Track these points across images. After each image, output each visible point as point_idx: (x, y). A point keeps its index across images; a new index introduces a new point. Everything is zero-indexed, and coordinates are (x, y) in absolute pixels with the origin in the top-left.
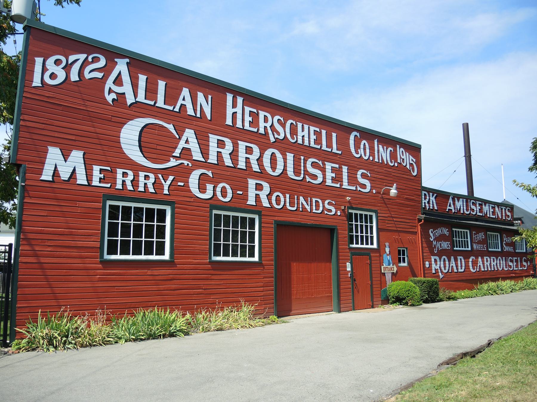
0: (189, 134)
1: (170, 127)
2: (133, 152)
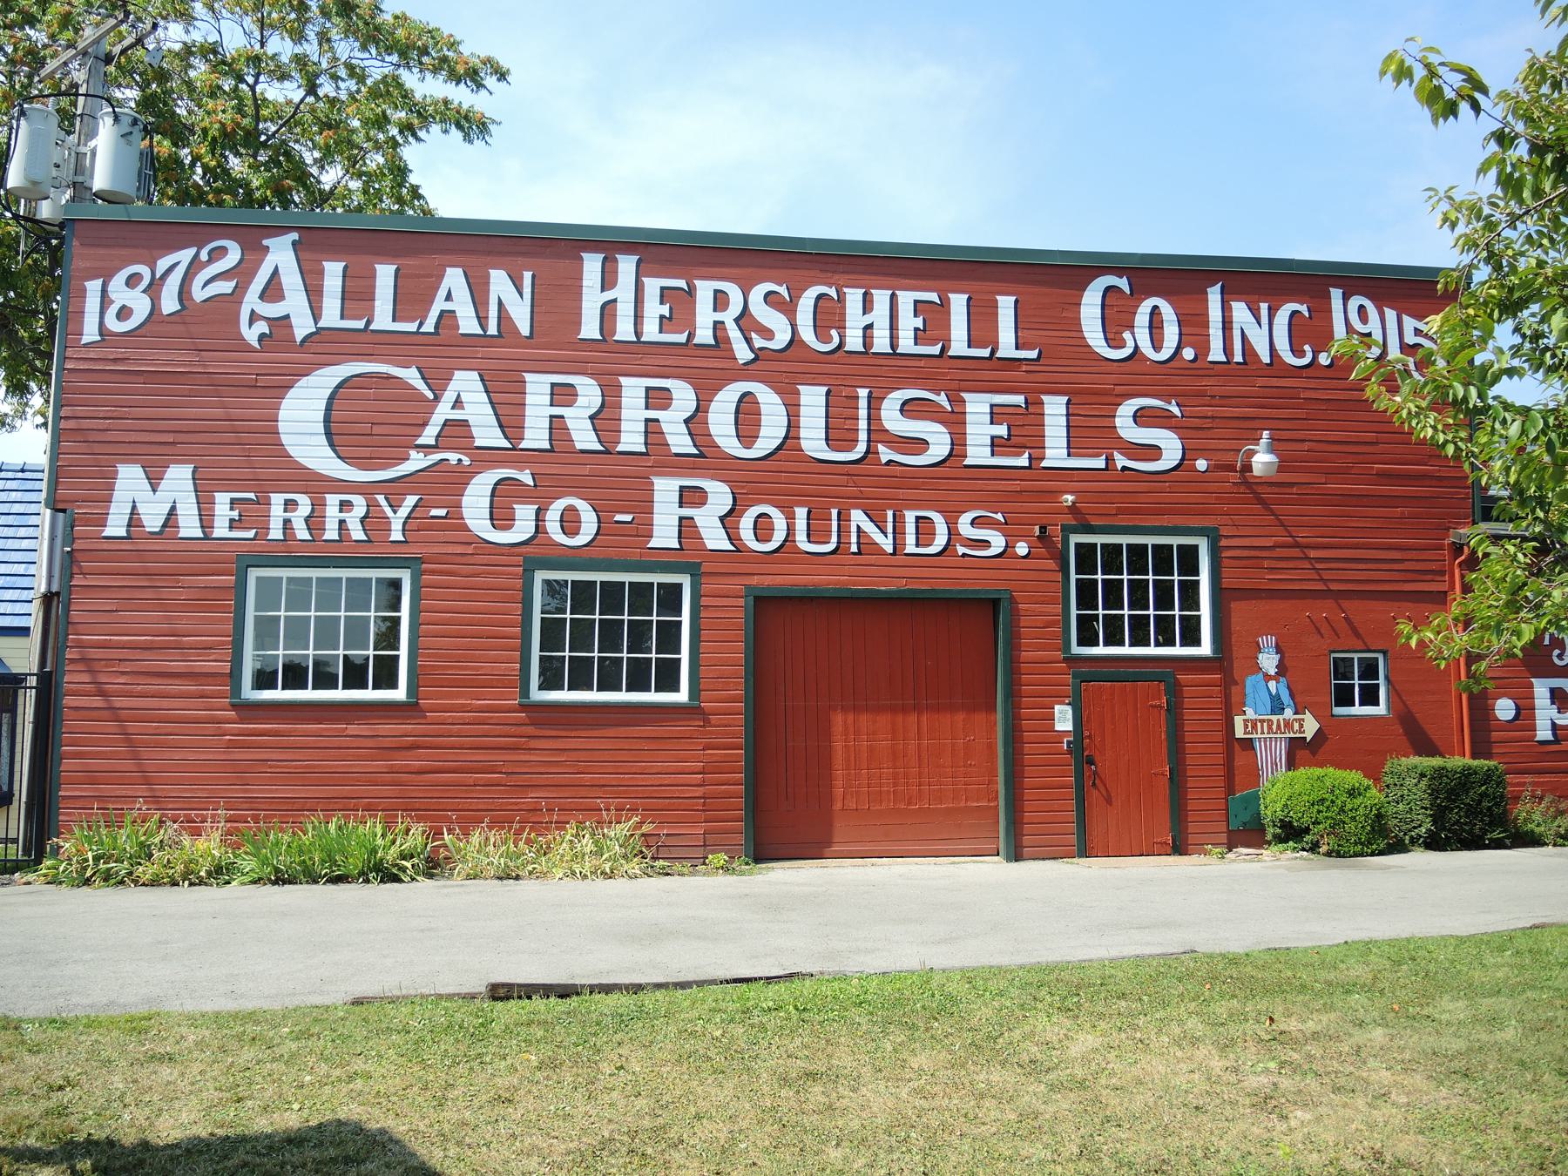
1: (411, 376)
2: (315, 454)
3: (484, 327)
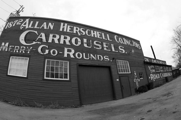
0: (43, 35)
1: (36, 32)
2: (23, 42)
3: (47, 28)
